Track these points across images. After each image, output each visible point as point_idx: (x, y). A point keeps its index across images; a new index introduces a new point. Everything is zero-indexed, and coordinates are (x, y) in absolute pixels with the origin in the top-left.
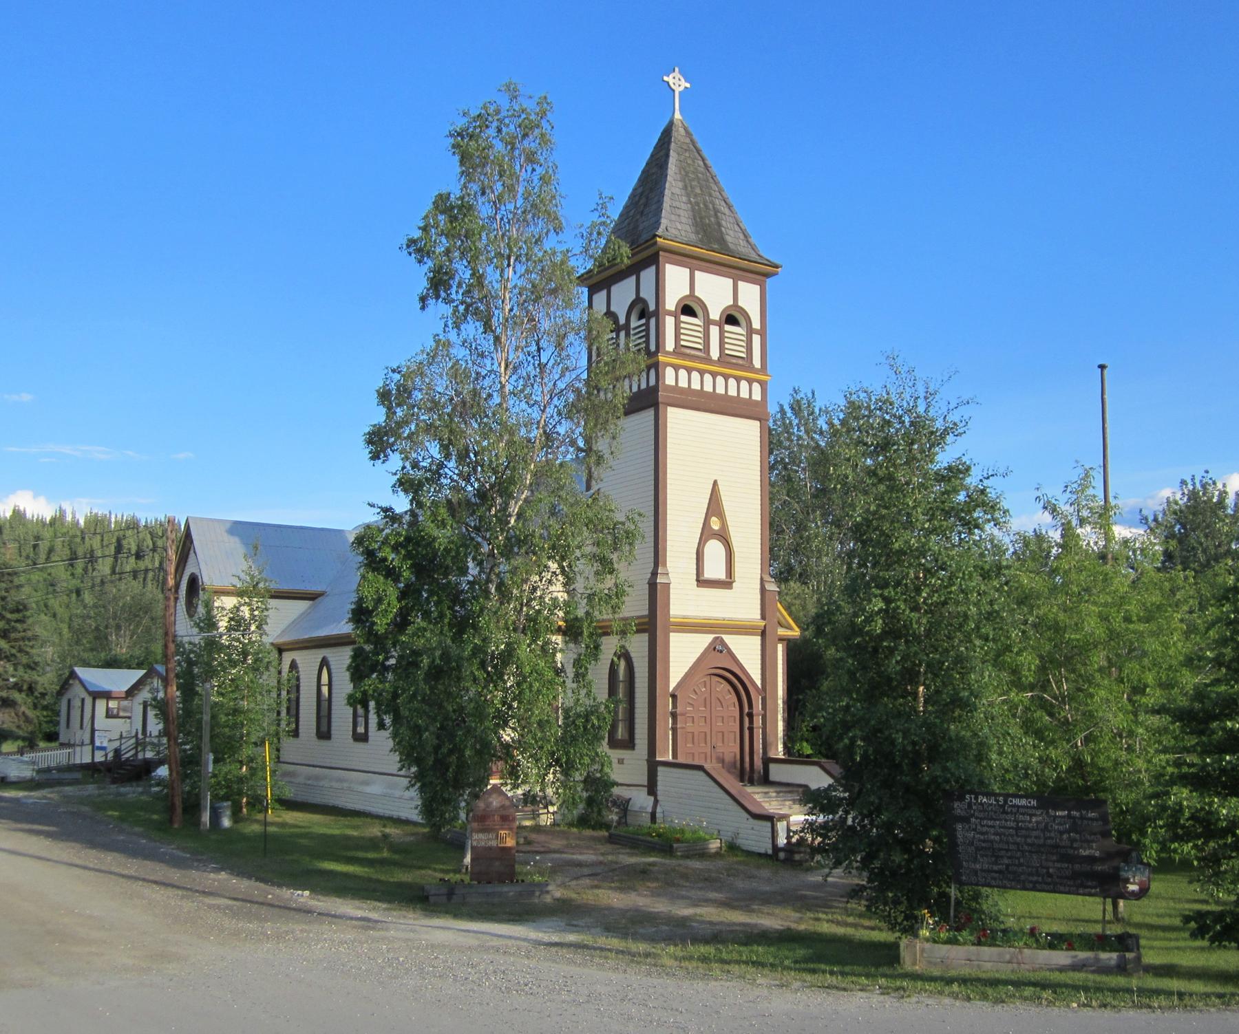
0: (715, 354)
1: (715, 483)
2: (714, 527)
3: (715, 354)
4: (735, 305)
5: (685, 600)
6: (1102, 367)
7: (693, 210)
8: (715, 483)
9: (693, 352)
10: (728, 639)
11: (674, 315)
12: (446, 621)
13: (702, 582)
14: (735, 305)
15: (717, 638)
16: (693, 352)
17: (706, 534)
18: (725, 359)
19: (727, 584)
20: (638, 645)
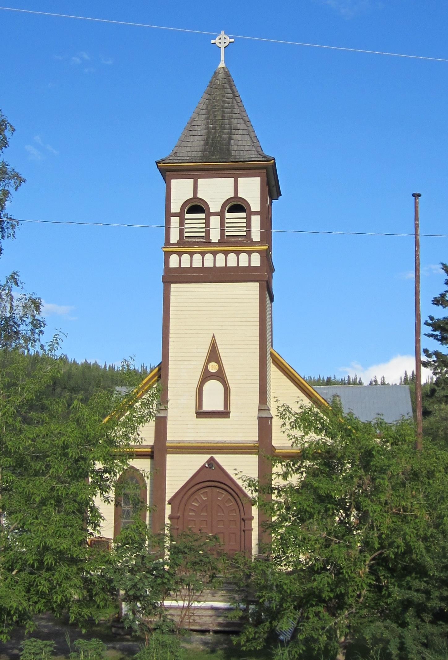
0: (215, 236)
1: (406, 372)
2: (214, 370)
3: (215, 236)
4: (195, 197)
5: (183, 426)
6: (416, 196)
7: (209, 133)
8: (406, 372)
9: (197, 240)
10: (220, 458)
11: (221, 214)
12: (194, 543)
13: (201, 414)
14: (195, 197)
15: (212, 457)
16: (197, 240)
17: (206, 376)
18: (224, 240)
19: (225, 414)
20: (143, 465)
